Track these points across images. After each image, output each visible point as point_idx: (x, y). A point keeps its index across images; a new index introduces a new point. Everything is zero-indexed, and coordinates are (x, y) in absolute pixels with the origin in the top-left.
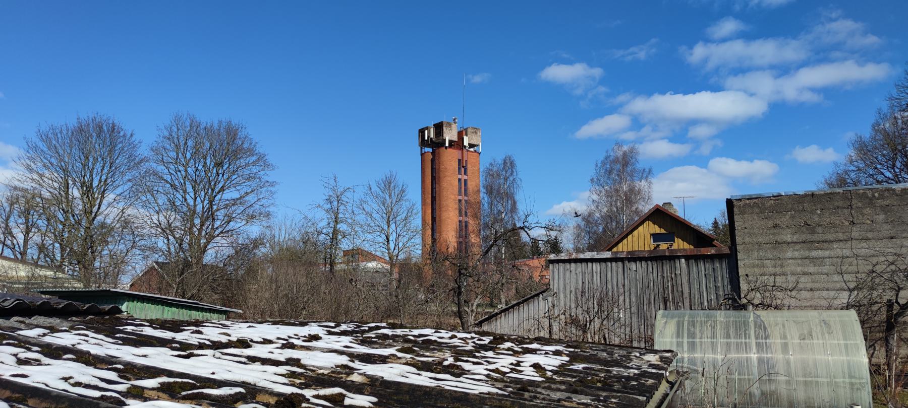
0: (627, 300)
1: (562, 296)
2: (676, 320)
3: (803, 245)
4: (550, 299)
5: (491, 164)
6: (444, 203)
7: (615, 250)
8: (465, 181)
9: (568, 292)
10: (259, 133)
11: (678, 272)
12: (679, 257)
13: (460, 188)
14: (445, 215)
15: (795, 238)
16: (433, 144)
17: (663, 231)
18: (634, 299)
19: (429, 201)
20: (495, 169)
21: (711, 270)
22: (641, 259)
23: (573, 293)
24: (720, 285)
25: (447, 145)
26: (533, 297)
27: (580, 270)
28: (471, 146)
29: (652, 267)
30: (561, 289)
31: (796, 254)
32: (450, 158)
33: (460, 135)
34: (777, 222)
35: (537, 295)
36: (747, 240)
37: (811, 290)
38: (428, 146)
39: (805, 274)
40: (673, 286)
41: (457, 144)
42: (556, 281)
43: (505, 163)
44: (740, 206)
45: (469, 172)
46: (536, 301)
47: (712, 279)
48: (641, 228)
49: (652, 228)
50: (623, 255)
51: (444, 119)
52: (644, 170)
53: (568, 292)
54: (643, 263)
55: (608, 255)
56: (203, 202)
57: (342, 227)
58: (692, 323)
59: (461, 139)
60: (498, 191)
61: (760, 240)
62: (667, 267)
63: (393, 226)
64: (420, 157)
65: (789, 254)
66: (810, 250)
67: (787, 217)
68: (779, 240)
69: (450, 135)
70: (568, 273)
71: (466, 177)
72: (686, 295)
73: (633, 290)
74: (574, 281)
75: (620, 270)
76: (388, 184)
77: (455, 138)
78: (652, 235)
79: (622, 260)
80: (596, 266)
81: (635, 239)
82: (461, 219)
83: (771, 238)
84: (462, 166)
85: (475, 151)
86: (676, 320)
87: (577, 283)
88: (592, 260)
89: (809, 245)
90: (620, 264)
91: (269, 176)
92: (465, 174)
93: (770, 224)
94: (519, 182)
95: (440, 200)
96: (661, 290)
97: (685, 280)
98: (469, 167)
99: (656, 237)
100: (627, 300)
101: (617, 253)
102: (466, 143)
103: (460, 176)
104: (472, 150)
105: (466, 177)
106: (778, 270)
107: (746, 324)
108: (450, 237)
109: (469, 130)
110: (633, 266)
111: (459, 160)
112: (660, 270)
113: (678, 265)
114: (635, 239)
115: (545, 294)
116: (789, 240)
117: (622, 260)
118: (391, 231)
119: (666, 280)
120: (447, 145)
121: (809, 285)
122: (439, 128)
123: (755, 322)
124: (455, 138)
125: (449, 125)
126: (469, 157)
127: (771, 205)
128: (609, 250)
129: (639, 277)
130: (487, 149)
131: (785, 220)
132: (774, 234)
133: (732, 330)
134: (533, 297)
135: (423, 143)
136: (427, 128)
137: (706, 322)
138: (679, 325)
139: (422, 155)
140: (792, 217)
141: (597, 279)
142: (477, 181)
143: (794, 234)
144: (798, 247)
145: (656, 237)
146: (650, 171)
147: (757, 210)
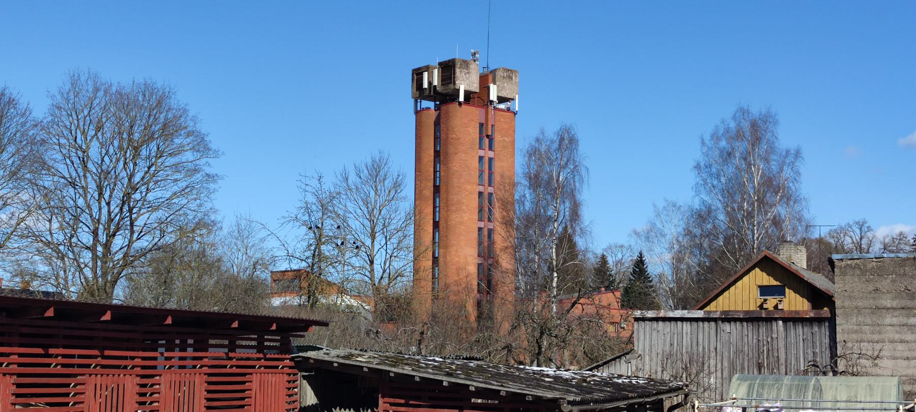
0: (719, 366)
1: (647, 358)
2: (748, 382)
3: (904, 312)
4: (634, 362)
5: (538, 140)
7: (708, 309)
8: (490, 159)
9: (654, 354)
10: (196, 99)
11: (775, 336)
12: (776, 319)
13: (481, 172)
14: (455, 218)
15: (895, 304)
16: (438, 94)
17: (779, 283)
18: (726, 364)
19: (429, 192)
20: (543, 148)
21: (810, 335)
22: (735, 320)
23: (660, 356)
24: (817, 351)
25: (462, 99)
26: (614, 359)
27: (668, 330)
28: (501, 100)
29: (748, 330)
30: (647, 351)
31: (895, 321)
32: (464, 122)
34: (878, 285)
35: (619, 357)
36: (847, 304)
37: (908, 358)
38: (429, 98)
39: (902, 341)
40: (768, 351)
42: (641, 342)
43: (562, 139)
44: (841, 268)
46: (618, 364)
47: (810, 345)
48: (746, 279)
49: (760, 277)
50: (717, 315)
51: (457, 55)
52: (788, 152)
53: (654, 354)
54: (738, 323)
55: (700, 314)
56: (108, 204)
57: (327, 249)
58: (762, 386)
60: (549, 182)
61: (860, 304)
62: (763, 329)
63: (379, 238)
64: (413, 117)
65: (888, 320)
66: (908, 316)
67: (888, 281)
68: (878, 305)
69: (466, 83)
70: (655, 334)
71: (491, 154)
72: (782, 361)
73: (726, 354)
74: (661, 342)
75: (713, 332)
76: (376, 172)
77: (475, 87)
78: (759, 287)
79: (715, 320)
80: (687, 326)
81: (739, 291)
82: (482, 224)
83: (870, 303)
84: (486, 136)
85: (508, 110)
86: (748, 382)
87: (664, 345)
88: (682, 319)
89: (908, 311)
90: (713, 324)
91: (212, 166)
92: (490, 148)
93: (871, 287)
94: (583, 172)
95: (447, 192)
96: (756, 355)
97: (781, 344)
98: (497, 138)
99: (765, 290)
100: (719, 366)
101: (709, 312)
102: (493, 97)
103: (481, 153)
104: (502, 106)
105: (491, 154)
106: (876, 337)
107: (806, 387)
108: (464, 257)
109: (499, 74)
110: (727, 327)
111: (481, 125)
112: (755, 332)
113: (774, 327)
114: (739, 291)
115: (628, 357)
116: (889, 305)
117: (715, 320)
118: (377, 247)
119: (761, 344)
120: (462, 99)
121: (906, 354)
122: (448, 69)
123: (814, 385)
124: (475, 87)
125: (466, 64)
126: (499, 122)
127: (873, 268)
128: (701, 308)
129: (733, 339)
130: (532, 119)
131: (885, 284)
132: (874, 298)
133: (794, 392)
134: (614, 359)
135: (420, 93)
136: (427, 68)
137: (773, 385)
138: (750, 388)
139: (417, 112)
140: (893, 281)
141: (686, 341)
142: (517, 165)
143: (893, 299)
144: (896, 313)
146: (798, 154)
147: (858, 272)
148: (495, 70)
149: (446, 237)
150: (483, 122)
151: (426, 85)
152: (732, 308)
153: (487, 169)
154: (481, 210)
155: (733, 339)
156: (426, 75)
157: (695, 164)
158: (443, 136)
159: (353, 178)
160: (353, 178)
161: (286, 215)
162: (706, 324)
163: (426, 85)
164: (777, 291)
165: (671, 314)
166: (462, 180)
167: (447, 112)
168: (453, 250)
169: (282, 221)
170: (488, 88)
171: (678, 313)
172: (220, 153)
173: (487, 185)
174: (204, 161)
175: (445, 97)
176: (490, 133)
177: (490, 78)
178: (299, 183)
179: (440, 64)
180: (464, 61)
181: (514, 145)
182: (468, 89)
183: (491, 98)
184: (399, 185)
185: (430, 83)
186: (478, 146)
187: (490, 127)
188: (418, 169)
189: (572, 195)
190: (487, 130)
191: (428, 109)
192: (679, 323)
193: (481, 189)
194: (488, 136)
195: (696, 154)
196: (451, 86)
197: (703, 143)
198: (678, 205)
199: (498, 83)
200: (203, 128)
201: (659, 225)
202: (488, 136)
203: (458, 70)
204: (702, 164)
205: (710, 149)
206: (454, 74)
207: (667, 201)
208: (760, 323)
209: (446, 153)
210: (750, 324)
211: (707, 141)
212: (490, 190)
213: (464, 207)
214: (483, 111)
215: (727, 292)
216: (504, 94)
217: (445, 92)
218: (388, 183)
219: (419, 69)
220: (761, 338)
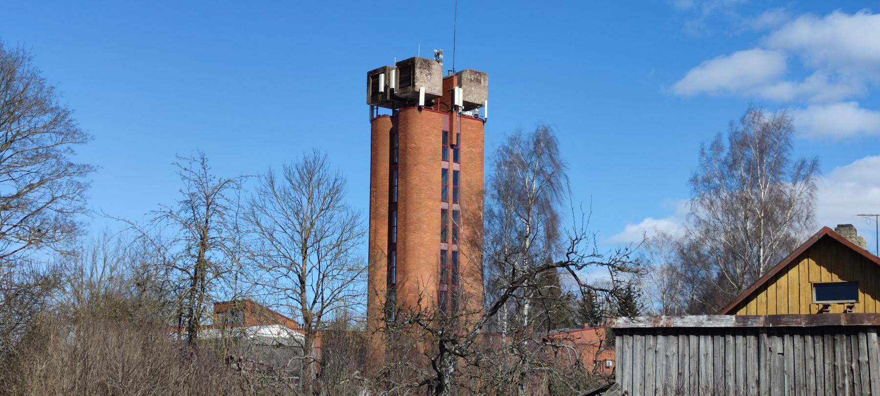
6: (413, 215)
7: (742, 312)
8: (456, 173)
11: (864, 358)
16: (394, 100)
17: (836, 279)
19: (384, 210)
22: (792, 331)
25: (422, 102)
28: (469, 106)
32: (426, 128)
33: (448, 84)
38: (385, 104)
40: (853, 385)
41: (442, 103)
42: (627, 370)
43: (537, 143)
45: (462, 157)
48: (793, 272)
50: (759, 323)
51: (418, 55)
54: (797, 338)
55: (728, 321)
57: (215, 256)
59: (449, 93)
62: (842, 348)
63: (313, 258)
69: (427, 85)
71: (456, 167)
74: (662, 369)
75: (752, 351)
76: (308, 175)
77: (438, 91)
79: (756, 332)
80: (706, 343)
84: (450, 145)
85: (476, 117)
88: (699, 331)
90: (752, 339)
91: (80, 154)
95: (405, 209)
98: (464, 148)
99: (823, 291)
101: (746, 318)
102: (459, 101)
103: (445, 165)
104: (469, 113)
105: (456, 167)
108: (423, 280)
109: (466, 76)
110: (777, 344)
111: (445, 134)
114: (782, 292)
117: (756, 332)
119: (839, 374)
120: (422, 102)
122: (407, 69)
124: (438, 91)
125: (427, 64)
126: (465, 128)
128: (732, 312)
129: (788, 365)
130: (499, 113)
135: (376, 98)
136: (384, 70)
139: (373, 121)
141: (706, 368)
145: (823, 291)
148: (461, 72)
149: (404, 259)
150: (448, 130)
151: (382, 89)
152: (783, 311)
153: (452, 186)
154: (444, 232)
155: (788, 365)
156: (382, 76)
157: (691, 177)
158: (401, 145)
159: (281, 182)
160: (281, 182)
161: (157, 209)
162: (740, 339)
163: (382, 89)
164: (843, 292)
165: (678, 323)
166: (423, 196)
167: (406, 119)
168: (412, 275)
169: (152, 216)
170: (453, 92)
171: (691, 321)
172: (89, 138)
173: (451, 201)
174: (65, 146)
175: (402, 101)
176: (455, 143)
177: (455, 80)
178: (178, 169)
179: (398, 64)
180: (425, 61)
181: (482, 157)
182: (429, 92)
183: (456, 103)
184: (338, 191)
185: (386, 87)
186: (441, 158)
187: (455, 135)
188: (373, 185)
189: (545, 207)
190: (451, 139)
191: (385, 116)
192: (693, 339)
193: (445, 205)
194: (452, 146)
195: (692, 165)
196: (410, 88)
197: (702, 153)
198: (668, 236)
199: (464, 86)
200: (60, 101)
201: (648, 257)
202: (452, 146)
203: (417, 71)
204: (700, 177)
205: (709, 160)
206: (414, 74)
207: (656, 231)
208: (837, 337)
209: (405, 165)
210: (818, 340)
211: (707, 151)
212: (456, 207)
213: (425, 226)
214: (447, 117)
215: (763, 294)
216: (471, 99)
217: (403, 96)
218: (324, 189)
219: (375, 71)
220: (838, 363)
